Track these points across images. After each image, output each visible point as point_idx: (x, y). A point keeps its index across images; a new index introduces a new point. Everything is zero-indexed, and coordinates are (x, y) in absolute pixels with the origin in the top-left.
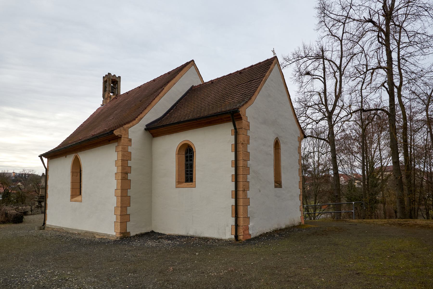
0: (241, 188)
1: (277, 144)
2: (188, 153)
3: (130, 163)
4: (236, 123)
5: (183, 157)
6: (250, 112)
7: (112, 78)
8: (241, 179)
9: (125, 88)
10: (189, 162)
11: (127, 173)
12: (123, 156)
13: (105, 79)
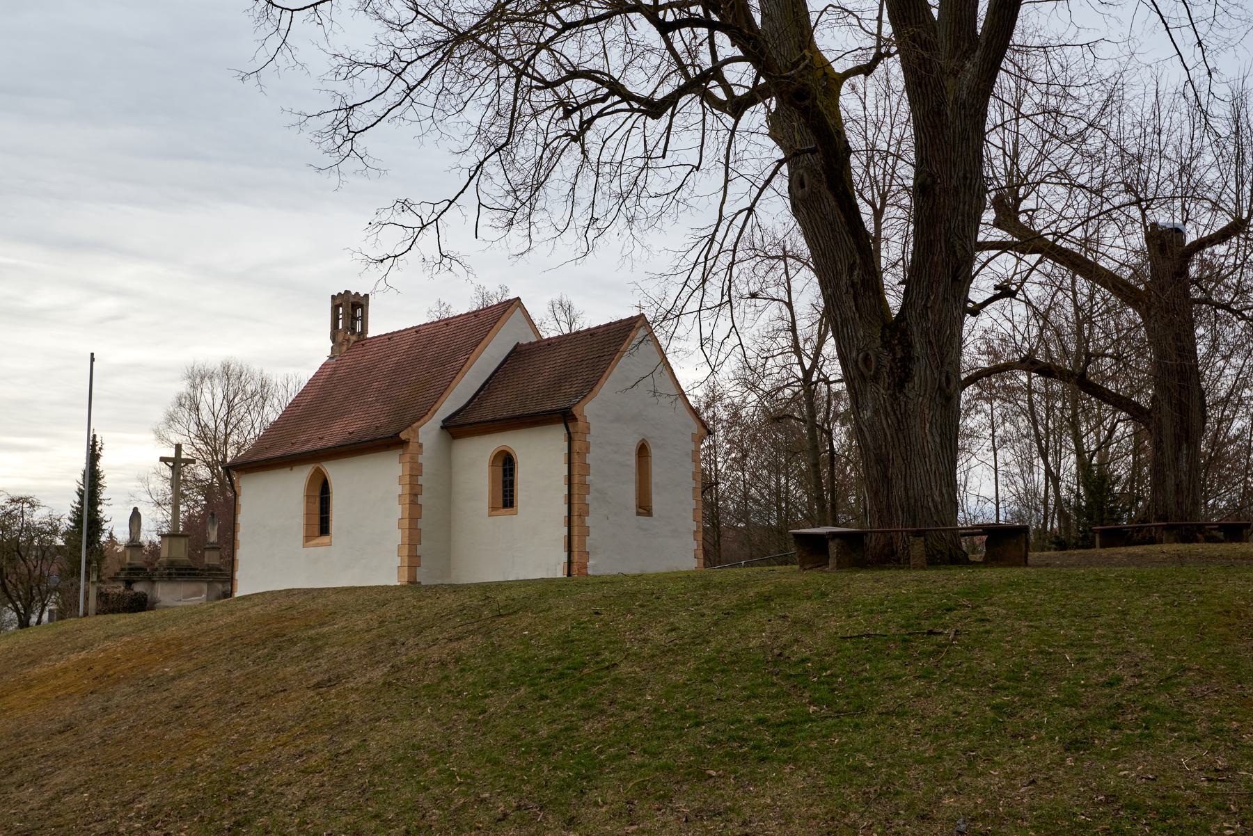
0: (575, 513)
1: (643, 451)
2: (506, 464)
3: (421, 480)
4: (570, 425)
5: (501, 469)
6: (590, 410)
7: (352, 300)
8: (575, 500)
9: (379, 324)
10: (508, 478)
11: (416, 495)
12: (411, 469)
13: (338, 302)
